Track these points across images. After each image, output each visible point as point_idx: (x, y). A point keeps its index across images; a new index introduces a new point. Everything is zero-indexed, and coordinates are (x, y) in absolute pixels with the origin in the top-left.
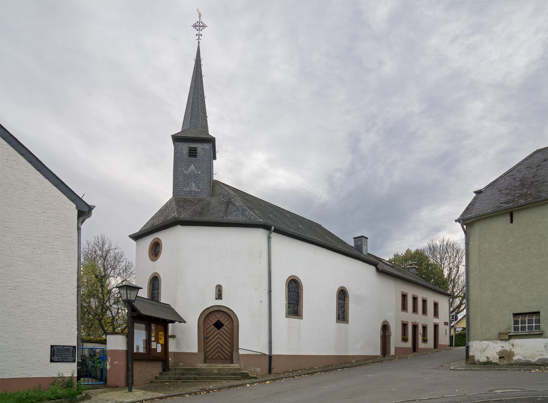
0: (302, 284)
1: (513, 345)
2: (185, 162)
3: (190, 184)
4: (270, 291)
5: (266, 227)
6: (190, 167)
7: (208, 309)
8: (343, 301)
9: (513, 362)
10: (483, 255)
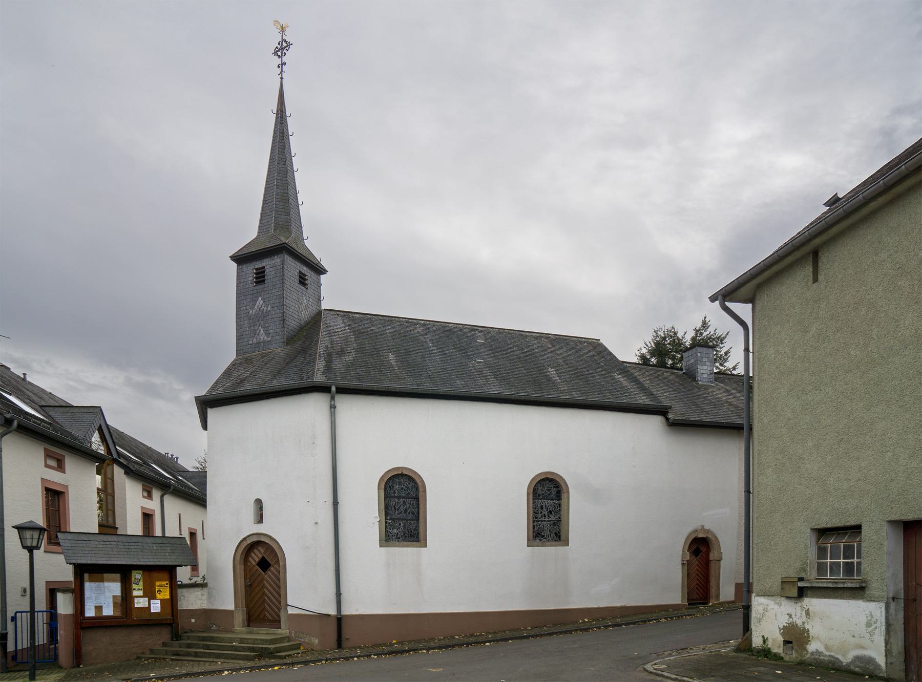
0: (422, 481)
1: (808, 613)
2: (250, 296)
3: (258, 331)
4: (335, 503)
5: (323, 389)
6: (258, 303)
7: (244, 539)
8: (556, 501)
9: (807, 656)
10: (765, 377)
